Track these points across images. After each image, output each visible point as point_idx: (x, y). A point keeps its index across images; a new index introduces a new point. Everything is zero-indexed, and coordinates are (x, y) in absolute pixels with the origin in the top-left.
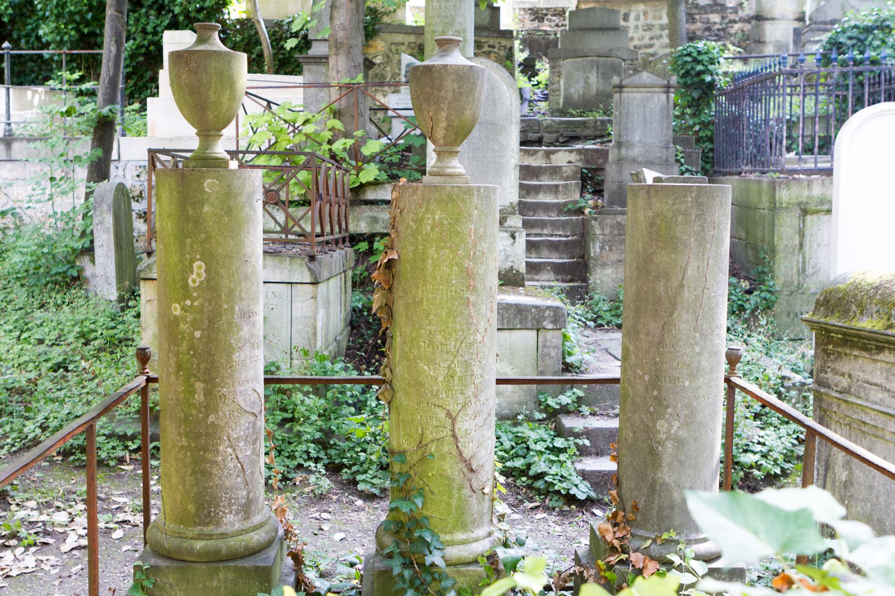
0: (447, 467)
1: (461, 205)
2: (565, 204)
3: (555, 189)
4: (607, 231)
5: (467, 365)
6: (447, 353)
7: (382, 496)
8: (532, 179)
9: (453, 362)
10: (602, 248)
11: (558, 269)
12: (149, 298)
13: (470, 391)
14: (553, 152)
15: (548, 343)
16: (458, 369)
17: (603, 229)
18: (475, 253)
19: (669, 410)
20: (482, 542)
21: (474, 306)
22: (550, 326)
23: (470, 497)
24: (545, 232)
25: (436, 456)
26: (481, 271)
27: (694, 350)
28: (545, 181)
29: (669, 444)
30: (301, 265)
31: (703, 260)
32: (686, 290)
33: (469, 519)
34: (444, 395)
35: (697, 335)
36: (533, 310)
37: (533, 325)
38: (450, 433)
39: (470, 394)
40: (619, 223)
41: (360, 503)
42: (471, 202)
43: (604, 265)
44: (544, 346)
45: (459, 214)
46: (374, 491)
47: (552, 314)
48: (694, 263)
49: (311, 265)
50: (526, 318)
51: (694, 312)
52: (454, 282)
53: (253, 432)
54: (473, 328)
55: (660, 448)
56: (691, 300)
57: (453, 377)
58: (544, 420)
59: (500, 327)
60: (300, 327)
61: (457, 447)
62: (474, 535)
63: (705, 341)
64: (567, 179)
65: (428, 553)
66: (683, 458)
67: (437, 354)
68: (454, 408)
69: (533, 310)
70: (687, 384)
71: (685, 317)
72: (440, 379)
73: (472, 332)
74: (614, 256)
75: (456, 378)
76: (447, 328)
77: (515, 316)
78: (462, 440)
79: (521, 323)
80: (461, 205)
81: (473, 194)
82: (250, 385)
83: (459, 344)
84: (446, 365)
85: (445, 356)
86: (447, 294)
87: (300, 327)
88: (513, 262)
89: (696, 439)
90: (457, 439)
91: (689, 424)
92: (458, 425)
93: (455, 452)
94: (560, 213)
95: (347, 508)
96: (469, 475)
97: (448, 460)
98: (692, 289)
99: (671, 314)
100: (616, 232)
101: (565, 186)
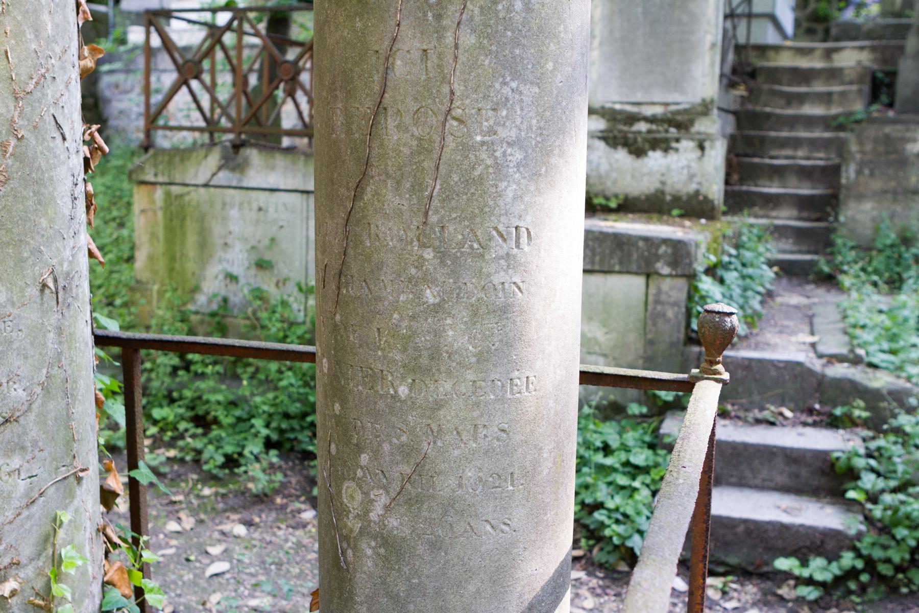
2: (835, 117)
3: (827, 98)
4: (869, 147)
8: (799, 84)
10: (859, 172)
11: (803, 203)
12: (142, 207)
14: (837, 50)
15: (663, 297)
17: (861, 143)
19: (364, 459)
22: (666, 270)
24: (800, 153)
27: (419, 296)
28: (819, 87)
29: (368, 548)
31: (440, 32)
32: (391, 123)
35: (429, 254)
36: (641, 244)
37: (639, 267)
40: (887, 136)
43: (861, 197)
44: (657, 302)
47: (669, 251)
48: (411, 43)
50: (629, 255)
51: (418, 187)
55: (350, 552)
56: (406, 151)
58: (643, 416)
59: (589, 267)
63: (454, 273)
64: (851, 83)
66: (401, 589)
69: (641, 244)
70: (403, 391)
71: (393, 200)
74: (877, 185)
77: (612, 253)
79: (621, 263)
88: (700, 183)
89: (435, 546)
91: (413, 502)
94: (827, 128)
98: (407, 120)
99: (359, 188)
100: (881, 149)
101: (843, 94)
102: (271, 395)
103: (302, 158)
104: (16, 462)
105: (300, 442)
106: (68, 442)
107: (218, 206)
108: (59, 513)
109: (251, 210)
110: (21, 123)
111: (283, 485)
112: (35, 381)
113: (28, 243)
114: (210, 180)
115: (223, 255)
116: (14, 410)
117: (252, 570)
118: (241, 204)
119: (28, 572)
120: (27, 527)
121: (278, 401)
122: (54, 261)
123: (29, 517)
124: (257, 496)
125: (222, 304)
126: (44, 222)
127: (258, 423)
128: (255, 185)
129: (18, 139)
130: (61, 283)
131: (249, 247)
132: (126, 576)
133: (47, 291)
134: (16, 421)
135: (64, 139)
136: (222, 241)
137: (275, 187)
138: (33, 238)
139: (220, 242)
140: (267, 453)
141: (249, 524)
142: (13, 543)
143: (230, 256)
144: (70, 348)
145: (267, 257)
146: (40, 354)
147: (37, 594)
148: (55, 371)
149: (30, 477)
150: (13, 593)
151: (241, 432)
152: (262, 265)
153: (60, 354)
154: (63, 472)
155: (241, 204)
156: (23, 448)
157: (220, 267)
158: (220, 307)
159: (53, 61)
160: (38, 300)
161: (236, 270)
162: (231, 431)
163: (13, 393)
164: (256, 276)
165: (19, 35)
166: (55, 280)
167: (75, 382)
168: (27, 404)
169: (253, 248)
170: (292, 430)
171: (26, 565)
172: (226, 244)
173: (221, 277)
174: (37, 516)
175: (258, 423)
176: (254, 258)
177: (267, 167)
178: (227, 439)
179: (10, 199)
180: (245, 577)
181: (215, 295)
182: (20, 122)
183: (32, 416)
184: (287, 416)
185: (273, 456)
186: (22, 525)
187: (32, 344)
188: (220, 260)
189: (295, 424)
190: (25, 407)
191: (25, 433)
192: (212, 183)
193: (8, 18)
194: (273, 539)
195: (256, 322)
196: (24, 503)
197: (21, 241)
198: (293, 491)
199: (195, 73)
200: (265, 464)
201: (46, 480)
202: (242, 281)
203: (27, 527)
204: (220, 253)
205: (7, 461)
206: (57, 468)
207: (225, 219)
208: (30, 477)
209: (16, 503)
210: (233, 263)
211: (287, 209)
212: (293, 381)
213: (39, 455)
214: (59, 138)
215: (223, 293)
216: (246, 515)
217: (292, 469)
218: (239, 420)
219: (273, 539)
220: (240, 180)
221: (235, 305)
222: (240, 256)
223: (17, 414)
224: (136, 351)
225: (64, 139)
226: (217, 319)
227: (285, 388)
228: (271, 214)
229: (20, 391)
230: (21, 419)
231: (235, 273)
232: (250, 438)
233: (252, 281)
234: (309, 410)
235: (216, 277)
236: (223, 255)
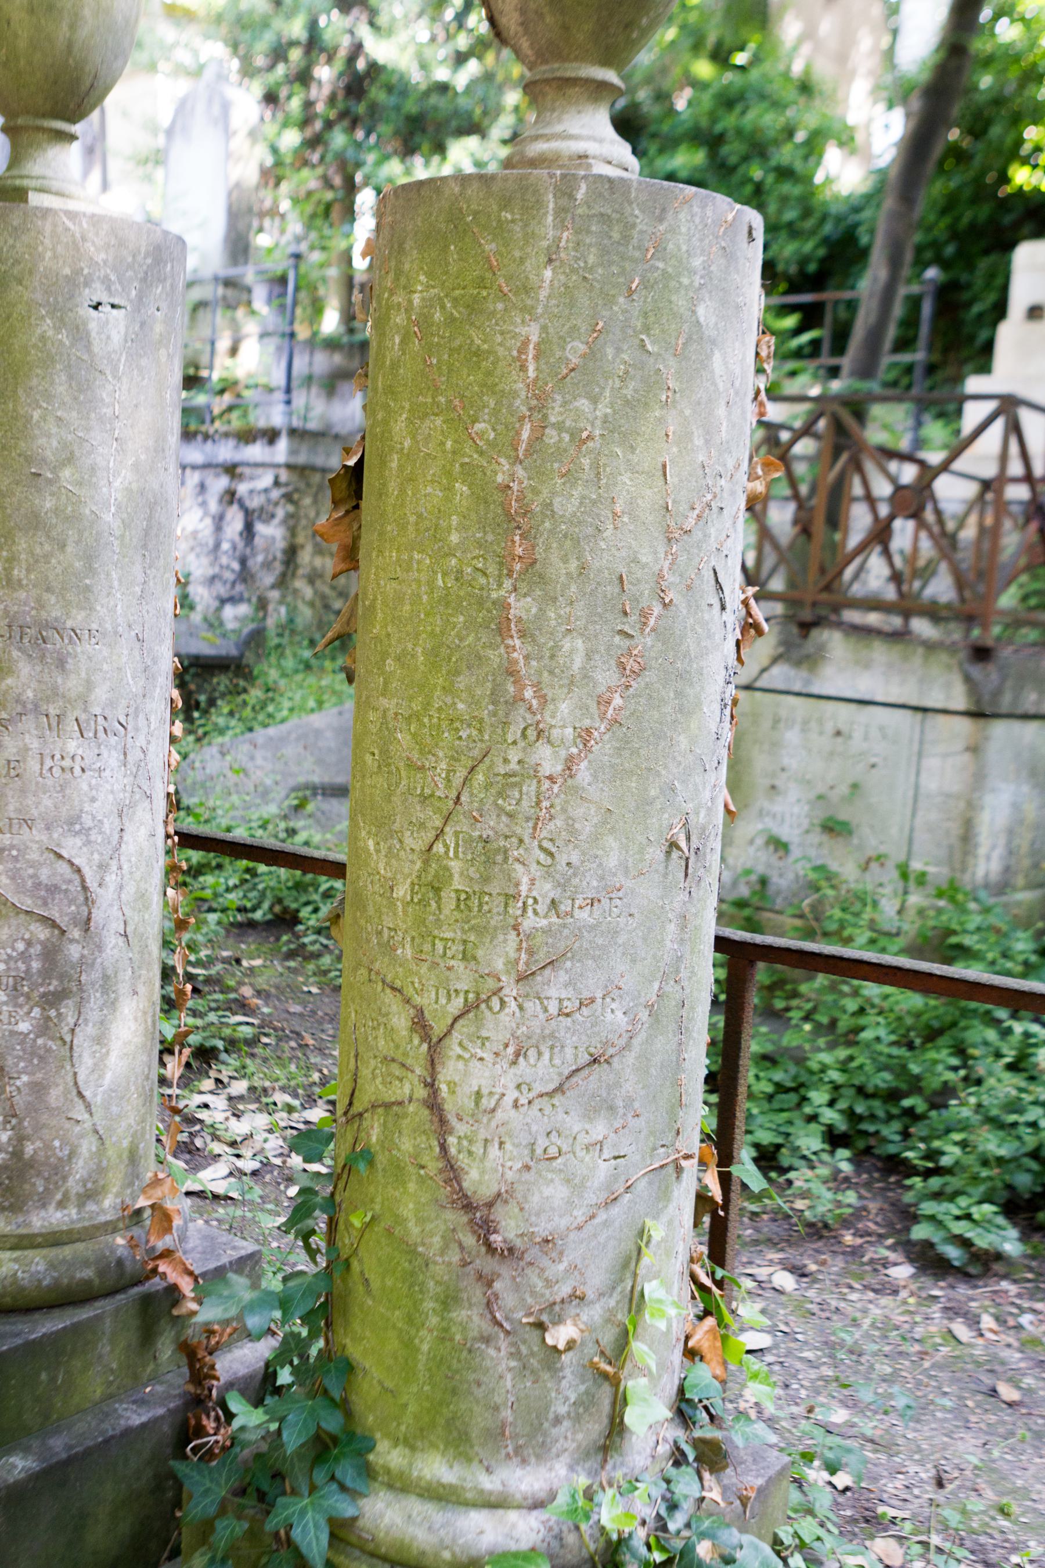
0: (408, 1209)
1: (490, 247)
5: (490, 855)
6: (424, 799)
7: (972, 1270)
9: (440, 834)
13: (501, 954)
16: (455, 866)
18: (538, 438)
20: (513, 1515)
21: (523, 634)
23: (487, 1340)
25: (381, 1160)
26: (567, 504)
30: (949, 667)
33: (480, 1421)
34: (409, 952)
38: (422, 1093)
39: (499, 965)
41: (902, 1272)
42: (529, 237)
45: (481, 283)
46: (953, 1253)
49: (976, 671)
52: (454, 538)
53: (46, 973)
54: (520, 718)
57: (437, 890)
60: (934, 816)
61: (444, 1147)
62: (489, 1483)
65: (305, 1490)
67: (396, 799)
68: (442, 1008)
72: (401, 891)
73: (514, 732)
75: (449, 898)
76: (427, 705)
78: (462, 1128)
80: (490, 247)
81: (539, 204)
82: (38, 835)
83: (461, 773)
84: (420, 845)
85: (419, 813)
86: (431, 583)
87: (934, 816)
90: (443, 1121)
92: (449, 1071)
93: (434, 1166)
95: (860, 1277)
96: (487, 1264)
97: (412, 1186)
102: (842, 1053)
103: (920, 650)
104: (599, 1130)
105: (885, 1141)
106: (673, 1106)
107: (766, 724)
108: (649, 1223)
109: (821, 733)
110: (671, 579)
111: (860, 1213)
112: (642, 1000)
113: (658, 774)
114: (756, 679)
115: (766, 805)
116: (606, 1043)
117: (808, 1354)
118: (806, 722)
119: (593, 1314)
120: (602, 1239)
121: (854, 1064)
122: (690, 807)
123: (606, 1224)
124: (811, 1225)
125: (758, 887)
126: (683, 742)
127: (819, 1097)
128: (824, 692)
129: (665, 605)
130: (695, 842)
131: (812, 795)
132: (719, 1344)
133: (675, 854)
134: (607, 1062)
135: (723, 608)
136: (766, 782)
137: (867, 697)
138: (666, 767)
139: (764, 782)
140: (832, 1153)
141: (800, 1272)
142: (578, 1262)
143: (778, 807)
144: (692, 952)
145: (843, 816)
146: (654, 956)
147: (602, 1353)
148: (670, 987)
149: (616, 1158)
150: (571, 1345)
151: (782, 1110)
152: (833, 828)
153: (679, 959)
154: (662, 1157)
155: (806, 722)
156: (612, 1108)
157: (760, 826)
158: (754, 893)
159: (723, 482)
160: (661, 868)
161: (785, 833)
162: (766, 1106)
163: (609, 1017)
164: (820, 845)
165: (685, 437)
166: (688, 839)
167: (692, 1008)
168: (626, 1036)
169: (820, 797)
170: (872, 1117)
171: (592, 1302)
172: (773, 787)
173: (760, 841)
174: (617, 1224)
175: (819, 1097)
176: (820, 815)
177: (857, 662)
178: (760, 1119)
179: (643, 701)
180: (799, 1365)
181: (748, 872)
182: (670, 578)
183: (630, 1058)
184: (861, 1091)
185: (843, 1161)
186: (595, 1235)
187: (645, 939)
188: (761, 814)
189: (878, 1107)
190: (622, 1042)
191: (618, 1085)
192: (758, 684)
193: (673, 412)
194: (842, 1305)
195: (814, 924)
196: (602, 1200)
197: (649, 769)
198: (872, 1226)
199: (911, 511)
200: (824, 1171)
201: (637, 1168)
202: (796, 852)
203: (602, 1239)
204: (762, 802)
205: (587, 1126)
206: (654, 1149)
207: (776, 745)
208: (616, 1158)
209: (591, 1198)
210: (783, 820)
211: (884, 737)
212: (882, 1032)
213: (633, 1123)
214: (717, 606)
215: (761, 869)
216: (791, 1254)
217: (868, 1185)
218: (780, 1088)
219: (842, 1305)
220: (808, 682)
221: (778, 893)
222: (796, 810)
223: (611, 1051)
224: (752, 963)
225: (723, 608)
226: (747, 912)
227: (868, 1045)
228: (857, 743)
229: (619, 1014)
230: (616, 1059)
231: (785, 838)
232: (799, 1122)
233: (812, 853)
234: (904, 1086)
235: (751, 842)
236: (766, 805)
